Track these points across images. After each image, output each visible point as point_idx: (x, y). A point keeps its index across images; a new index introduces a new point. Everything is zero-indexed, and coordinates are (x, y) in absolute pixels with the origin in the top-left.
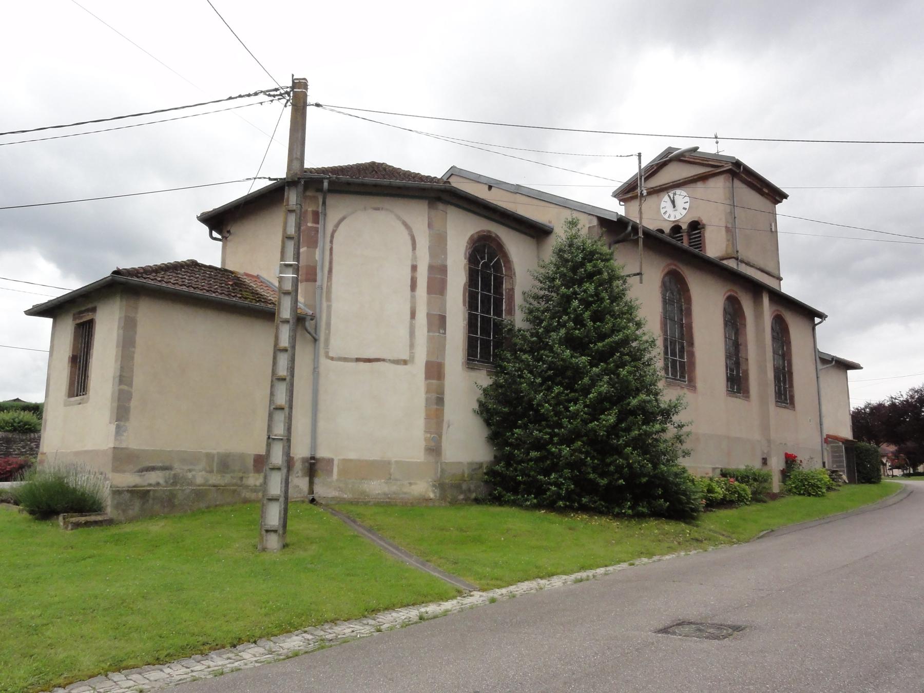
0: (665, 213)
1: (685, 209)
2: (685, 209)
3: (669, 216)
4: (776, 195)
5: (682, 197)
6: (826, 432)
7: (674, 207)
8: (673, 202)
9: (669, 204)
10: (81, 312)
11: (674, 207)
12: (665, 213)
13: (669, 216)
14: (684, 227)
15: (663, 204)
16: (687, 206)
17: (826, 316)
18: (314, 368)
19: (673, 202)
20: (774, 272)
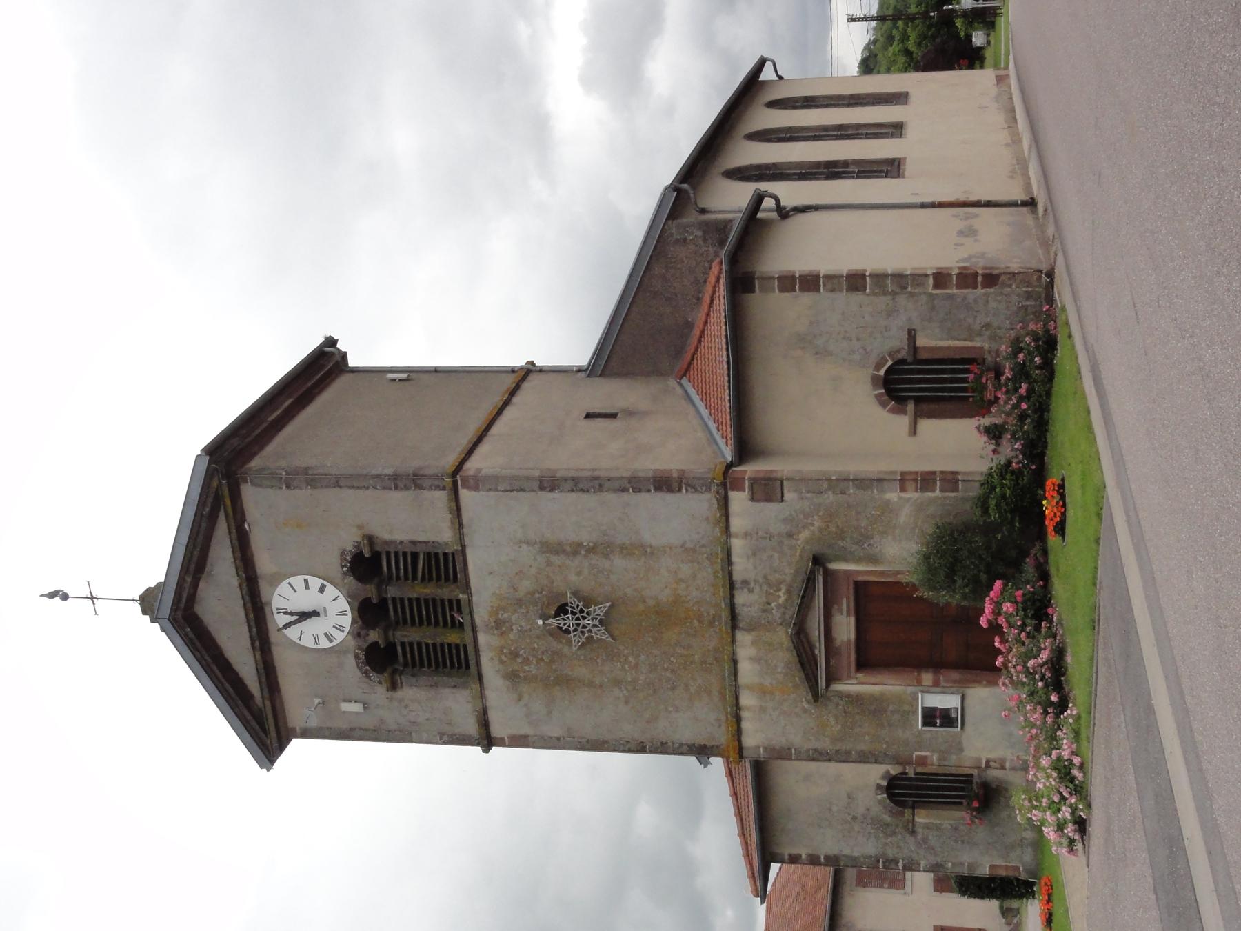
0: (329, 637)
1: (322, 589)
2: (322, 589)
3: (339, 628)
4: (323, 367)
5: (289, 595)
6: (978, 80)
7: (315, 614)
8: (304, 616)
9: (310, 626)
10: (601, 548)
11: (315, 614)
12: (329, 637)
13: (339, 628)
14: (370, 591)
15: (308, 642)
16: (315, 582)
17: (331, 342)
18: (658, 488)
19: (304, 616)
20: (510, 381)
